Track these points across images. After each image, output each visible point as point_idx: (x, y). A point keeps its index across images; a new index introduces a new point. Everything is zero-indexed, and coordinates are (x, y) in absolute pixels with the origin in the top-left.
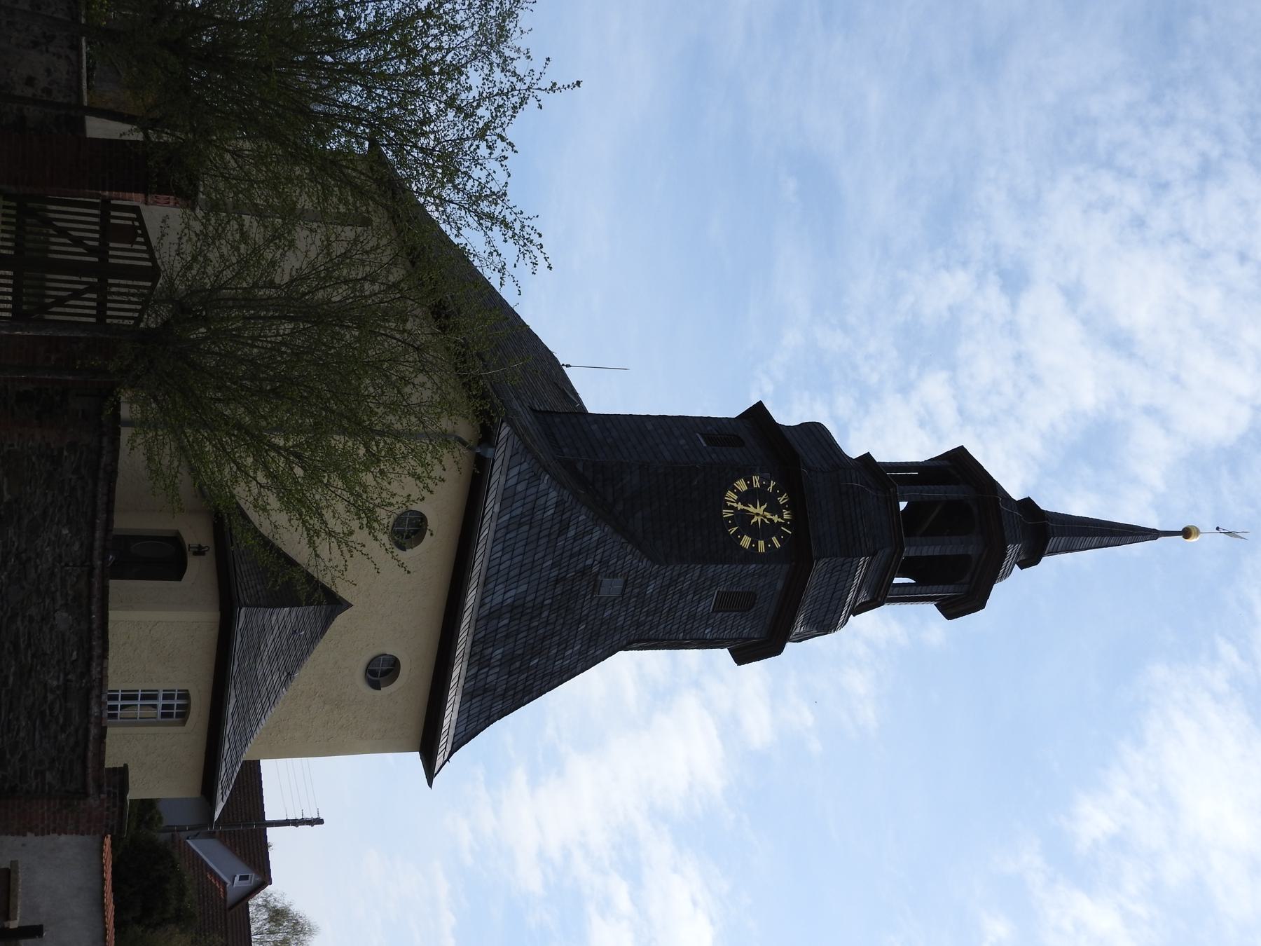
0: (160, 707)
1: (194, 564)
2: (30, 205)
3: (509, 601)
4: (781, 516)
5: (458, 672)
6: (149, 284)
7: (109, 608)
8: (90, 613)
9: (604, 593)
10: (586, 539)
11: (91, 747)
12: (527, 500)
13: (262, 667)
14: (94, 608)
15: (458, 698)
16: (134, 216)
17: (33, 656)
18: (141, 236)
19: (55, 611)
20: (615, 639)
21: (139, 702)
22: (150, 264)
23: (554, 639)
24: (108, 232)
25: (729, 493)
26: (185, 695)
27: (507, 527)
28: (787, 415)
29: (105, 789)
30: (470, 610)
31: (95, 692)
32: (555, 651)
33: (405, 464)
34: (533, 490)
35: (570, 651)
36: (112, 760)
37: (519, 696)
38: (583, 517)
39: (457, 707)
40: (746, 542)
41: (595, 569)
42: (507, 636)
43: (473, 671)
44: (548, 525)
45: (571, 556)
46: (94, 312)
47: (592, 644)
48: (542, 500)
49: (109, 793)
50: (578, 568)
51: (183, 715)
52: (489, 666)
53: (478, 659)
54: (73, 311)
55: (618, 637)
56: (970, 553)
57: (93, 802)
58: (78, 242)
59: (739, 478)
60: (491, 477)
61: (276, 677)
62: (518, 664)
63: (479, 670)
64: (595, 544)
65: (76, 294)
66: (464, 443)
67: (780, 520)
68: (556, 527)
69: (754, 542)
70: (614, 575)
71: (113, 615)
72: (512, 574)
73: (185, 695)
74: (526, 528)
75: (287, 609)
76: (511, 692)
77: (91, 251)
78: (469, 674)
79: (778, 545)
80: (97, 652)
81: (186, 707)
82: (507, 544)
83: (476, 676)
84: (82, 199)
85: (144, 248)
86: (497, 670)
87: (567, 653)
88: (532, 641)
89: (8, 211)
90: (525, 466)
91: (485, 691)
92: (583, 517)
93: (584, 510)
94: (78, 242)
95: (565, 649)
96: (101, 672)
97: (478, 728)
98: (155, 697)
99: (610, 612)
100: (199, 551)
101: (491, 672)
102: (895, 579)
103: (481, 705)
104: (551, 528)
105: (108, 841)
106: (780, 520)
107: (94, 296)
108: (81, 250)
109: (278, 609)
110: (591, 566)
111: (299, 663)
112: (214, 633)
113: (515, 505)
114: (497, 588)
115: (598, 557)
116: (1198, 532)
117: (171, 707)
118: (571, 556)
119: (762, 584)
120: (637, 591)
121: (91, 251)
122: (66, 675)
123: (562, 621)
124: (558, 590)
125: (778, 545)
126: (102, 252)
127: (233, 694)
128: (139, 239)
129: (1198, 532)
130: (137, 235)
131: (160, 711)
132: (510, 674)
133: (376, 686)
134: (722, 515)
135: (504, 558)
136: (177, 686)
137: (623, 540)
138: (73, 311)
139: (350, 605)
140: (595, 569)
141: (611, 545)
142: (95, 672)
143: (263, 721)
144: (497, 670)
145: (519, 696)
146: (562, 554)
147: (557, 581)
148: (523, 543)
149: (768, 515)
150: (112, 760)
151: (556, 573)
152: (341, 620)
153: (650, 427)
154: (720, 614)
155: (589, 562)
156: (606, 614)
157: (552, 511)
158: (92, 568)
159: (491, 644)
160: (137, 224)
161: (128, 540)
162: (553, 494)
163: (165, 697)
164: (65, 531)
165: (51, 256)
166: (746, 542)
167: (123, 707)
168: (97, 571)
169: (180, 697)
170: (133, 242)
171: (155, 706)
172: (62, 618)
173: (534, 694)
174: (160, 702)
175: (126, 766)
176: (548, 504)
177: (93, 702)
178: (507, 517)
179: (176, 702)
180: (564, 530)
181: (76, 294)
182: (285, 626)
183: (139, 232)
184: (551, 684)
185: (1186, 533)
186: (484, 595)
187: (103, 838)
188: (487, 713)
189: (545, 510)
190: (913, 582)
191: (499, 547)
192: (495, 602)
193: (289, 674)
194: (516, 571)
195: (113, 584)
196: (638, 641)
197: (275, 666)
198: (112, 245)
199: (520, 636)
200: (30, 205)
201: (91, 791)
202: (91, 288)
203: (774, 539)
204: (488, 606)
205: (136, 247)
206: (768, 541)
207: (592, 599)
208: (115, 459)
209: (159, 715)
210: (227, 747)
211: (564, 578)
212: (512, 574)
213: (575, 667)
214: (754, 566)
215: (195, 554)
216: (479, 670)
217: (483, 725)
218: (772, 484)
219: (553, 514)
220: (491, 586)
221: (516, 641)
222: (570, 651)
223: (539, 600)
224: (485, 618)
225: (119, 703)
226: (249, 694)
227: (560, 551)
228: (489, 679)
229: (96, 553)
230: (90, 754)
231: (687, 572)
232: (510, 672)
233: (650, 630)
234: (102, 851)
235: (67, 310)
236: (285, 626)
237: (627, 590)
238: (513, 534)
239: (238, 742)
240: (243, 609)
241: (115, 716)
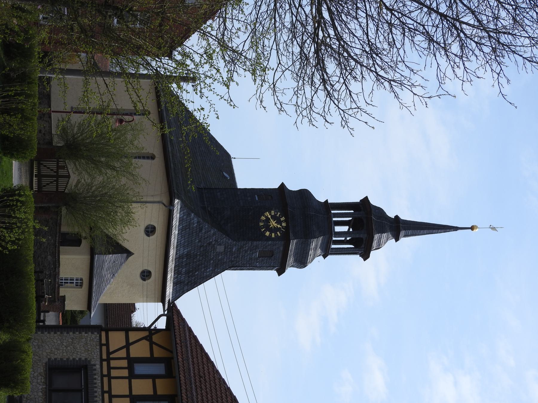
0: (75, 283)
1: (84, 242)
2: (41, 162)
3: (185, 253)
4: (281, 225)
5: (170, 276)
7: (89, 324)
8: (56, 256)
9: (218, 250)
10: (209, 233)
11: (56, 289)
12: (187, 221)
13: (104, 272)
14: (57, 255)
15: (172, 284)
17: (43, 267)
19: (48, 256)
20: (224, 266)
21: (69, 281)
22: (68, 174)
23: (202, 266)
24: (58, 167)
25: (263, 217)
26: (81, 279)
27: (182, 229)
28: (293, 186)
29: (60, 300)
30: (172, 256)
31: (57, 276)
32: (203, 270)
34: (188, 218)
35: (209, 270)
36: (61, 294)
37: (193, 285)
38: (206, 226)
39: (172, 287)
40: (267, 234)
41: (213, 243)
42: (186, 264)
43: (176, 276)
44: (195, 229)
45: (204, 239)
46: (55, 188)
47: (216, 267)
48: (192, 221)
49: (61, 302)
50: (207, 242)
51: (81, 286)
52: (181, 274)
53: (177, 271)
54: (52, 186)
55: (225, 265)
56: (361, 237)
57: (57, 303)
58: (52, 170)
59: (266, 212)
60: (173, 215)
61: (109, 275)
62: (191, 274)
63: (178, 275)
64: (212, 235)
65: (51, 182)
66: (165, 205)
67: (280, 227)
68: (198, 230)
69: (271, 234)
70: (220, 245)
71: (61, 256)
72: (185, 244)
73: (81, 279)
74: (188, 230)
75: (111, 255)
76: (190, 283)
77: (55, 172)
78: (175, 277)
79: (279, 235)
80: (57, 266)
81: (82, 283)
82: (182, 235)
83: (177, 277)
86: (184, 275)
87: (207, 271)
88: (195, 266)
90: (185, 211)
91: (181, 283)
92: (206, 226)
93: (207, 224)
94: (52, 170)
95: (207, 269)
96: (58, 271)
97: (180, 295)
98: (73, 280)
99: (221, 257)
100: (85, 238)
101: (182, 276)
103: (180, 287)
104: (196, 230)
105: (61, 314)
106: (280, 227)
107: (56, 183)
109: (108, 255)
110: (212, 242)
111: (117, 271)
112: (89, 261)
113: (183, 223)
114: (181, 249)
115: (214, 239)
116: (477, 227)
117: (78, 283)
118: (204, 239)
119: (275, 248)
120: (229, 250)
122: (50, 271)
123: (204, 260)
124: (202, 249)
125: (279, 235)
126: (57, 172)
127: (95, 279)
128: (66, 169)
129: (477, 227)
131: (75, 284)
132: (189, 277)
133: (144, 280)
134: (259, 225)
135: (182, 239)
136: (79, 276)
137: (222, 234)
138: (52, 186)
139: (133, 254)
140: (213, 243)
141: (218, 235)
142: (57, 270)
143: (106, 288)
144: (184, 275)
145: (193, 285)
146: (201, 238)
147: (201, 247)
148: (188, 234)
149: (276, 224)
150: (61, 294)
151: (200, 244)
152: (131, 258)
153: (239, 193)
154: (261, 258)
155: (211, 240)
156: (220, 258)
157: (196, 224)
158: (56, 246)
159: (181, 267)
161: (64, 235)
162: (196, 219)
163: (76, 280)
164: (50, 238)
166: (267, 234)
167: (65, 283)
168: (57, 247)
169: (80, 280)
170: (64, 169)
171: (73, 283)
172: (49, 258)
173: (198, 284)
174: (75, 281)
175: (65, 295)
176: (194, 222)
177: (57, 278)
178: (181, 226)
179: (79, 281)
180: (201, 230)
181: (51, 182)
182: (111, 260)
184: (204, 281)
185: (472, 228)
186: (177, 251)
187: (60, 313)
188: (182, 290)
189: (194, 224)
190: (353, 247)
191: (180, 236)
192: (181, 253)
193: (113, 275)
194: (187, 243)
195: (61, 247)
196: (233, 267)
197: (108, 272)
199: (191, 264)
201: (56, 300)
202: (55, 181)
203: (278, 233)
204: (178, 254)
206: (276, 233)
207: (214, 253)
208: (61, 221)
209: (75, 285)
210: (94, 295)
211: (203, 246)
212: (185, 244)
213: (211, 275)
214: (270, 242)
215: (84, 239)
216: (178, 275)
217: (181, 294)
218: (279, 213)
219: (196, 225)
220: (179, 248)
221: (189, 266)
222: (209, 270)
223: (196, 252)
224: (178, 258)
225: (64, 281)
226: (100, 280)
227: (200, 237)
228: (182, 278)
229: (57, 243)
230: (56, 291)
231: (246, 244)
232: (188, 276)
233: (236, 263)
234: (59, 317)
235: (53, 184)
236: (111, 260)
237: (226, 250)
238: (184, 232)
239: (98, 294)
240: (96, 255)
241: (62, 285)
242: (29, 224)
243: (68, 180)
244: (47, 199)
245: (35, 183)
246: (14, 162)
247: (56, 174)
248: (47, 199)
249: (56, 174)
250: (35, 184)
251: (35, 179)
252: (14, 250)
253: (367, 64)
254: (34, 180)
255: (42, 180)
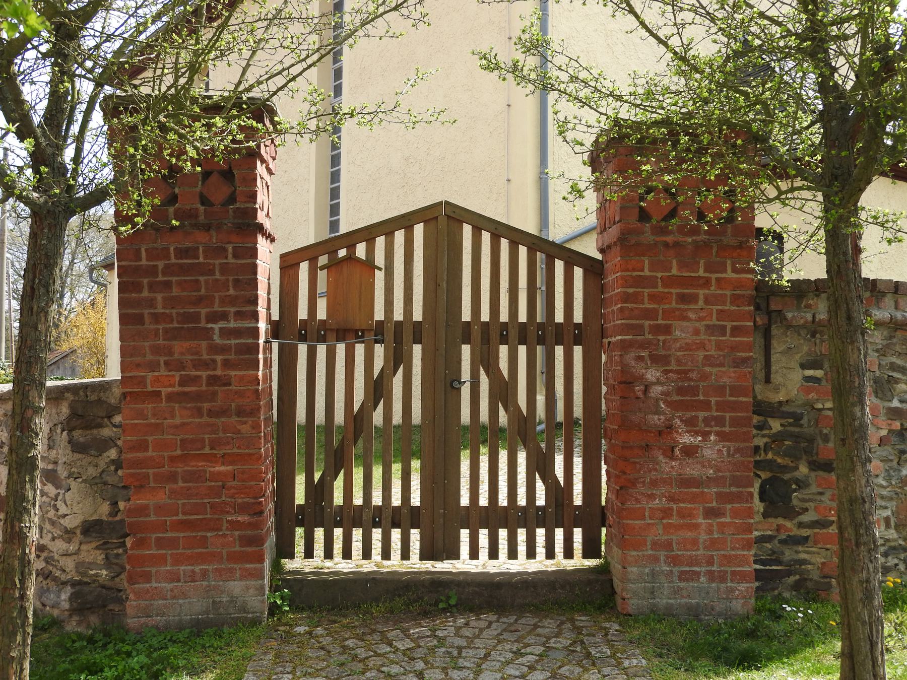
2: (300, 498)
6: (467, 229)
16: (304, 267)
18: (352, 247)
22: (419, 230)
33: (675, 63)
46: (503, 501)
77: (399, 358)
84: (190, 326)
85: (380, 241)
89: (338, 546)
102: (562, 263)
108: (398, 381)
121: (399, 358)
128: (361, 250)
130: (351, 258)
160: (323, 260)
165: (416, 417)
170: (369, 265)
183: (342, 253)
198: (465, 501)
200: (300, 498)
205: (380, 260)
242: (819, 128)
243: (480, 223)
244: (687, 439)
245: (493, 554)
246: (739, 608)
247: (417, 349)
248: (687, 439)
249: (417, 349)
250: (541, 551)
251: (474, 554)
252: (810, 394)
253: (804, 250)
254: (483, 565)
255: (377, 472)
